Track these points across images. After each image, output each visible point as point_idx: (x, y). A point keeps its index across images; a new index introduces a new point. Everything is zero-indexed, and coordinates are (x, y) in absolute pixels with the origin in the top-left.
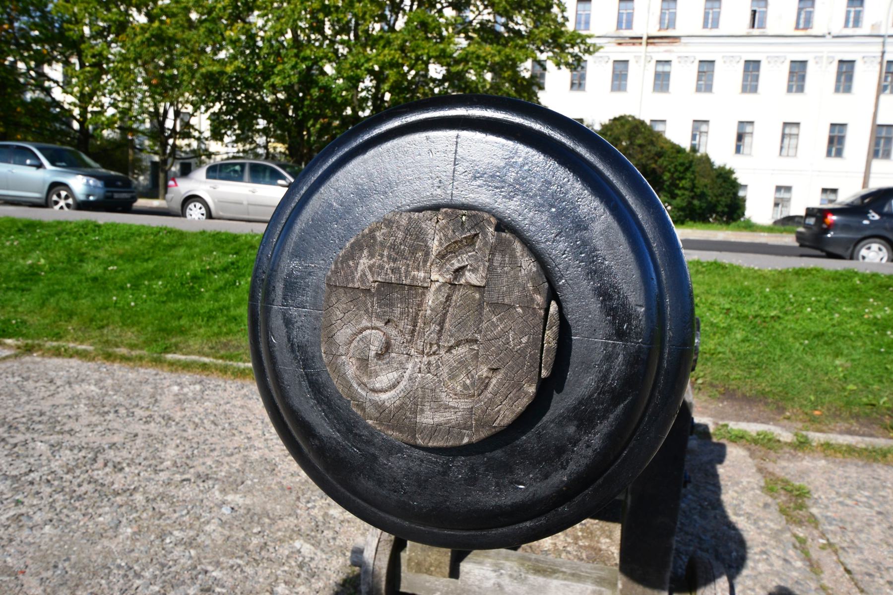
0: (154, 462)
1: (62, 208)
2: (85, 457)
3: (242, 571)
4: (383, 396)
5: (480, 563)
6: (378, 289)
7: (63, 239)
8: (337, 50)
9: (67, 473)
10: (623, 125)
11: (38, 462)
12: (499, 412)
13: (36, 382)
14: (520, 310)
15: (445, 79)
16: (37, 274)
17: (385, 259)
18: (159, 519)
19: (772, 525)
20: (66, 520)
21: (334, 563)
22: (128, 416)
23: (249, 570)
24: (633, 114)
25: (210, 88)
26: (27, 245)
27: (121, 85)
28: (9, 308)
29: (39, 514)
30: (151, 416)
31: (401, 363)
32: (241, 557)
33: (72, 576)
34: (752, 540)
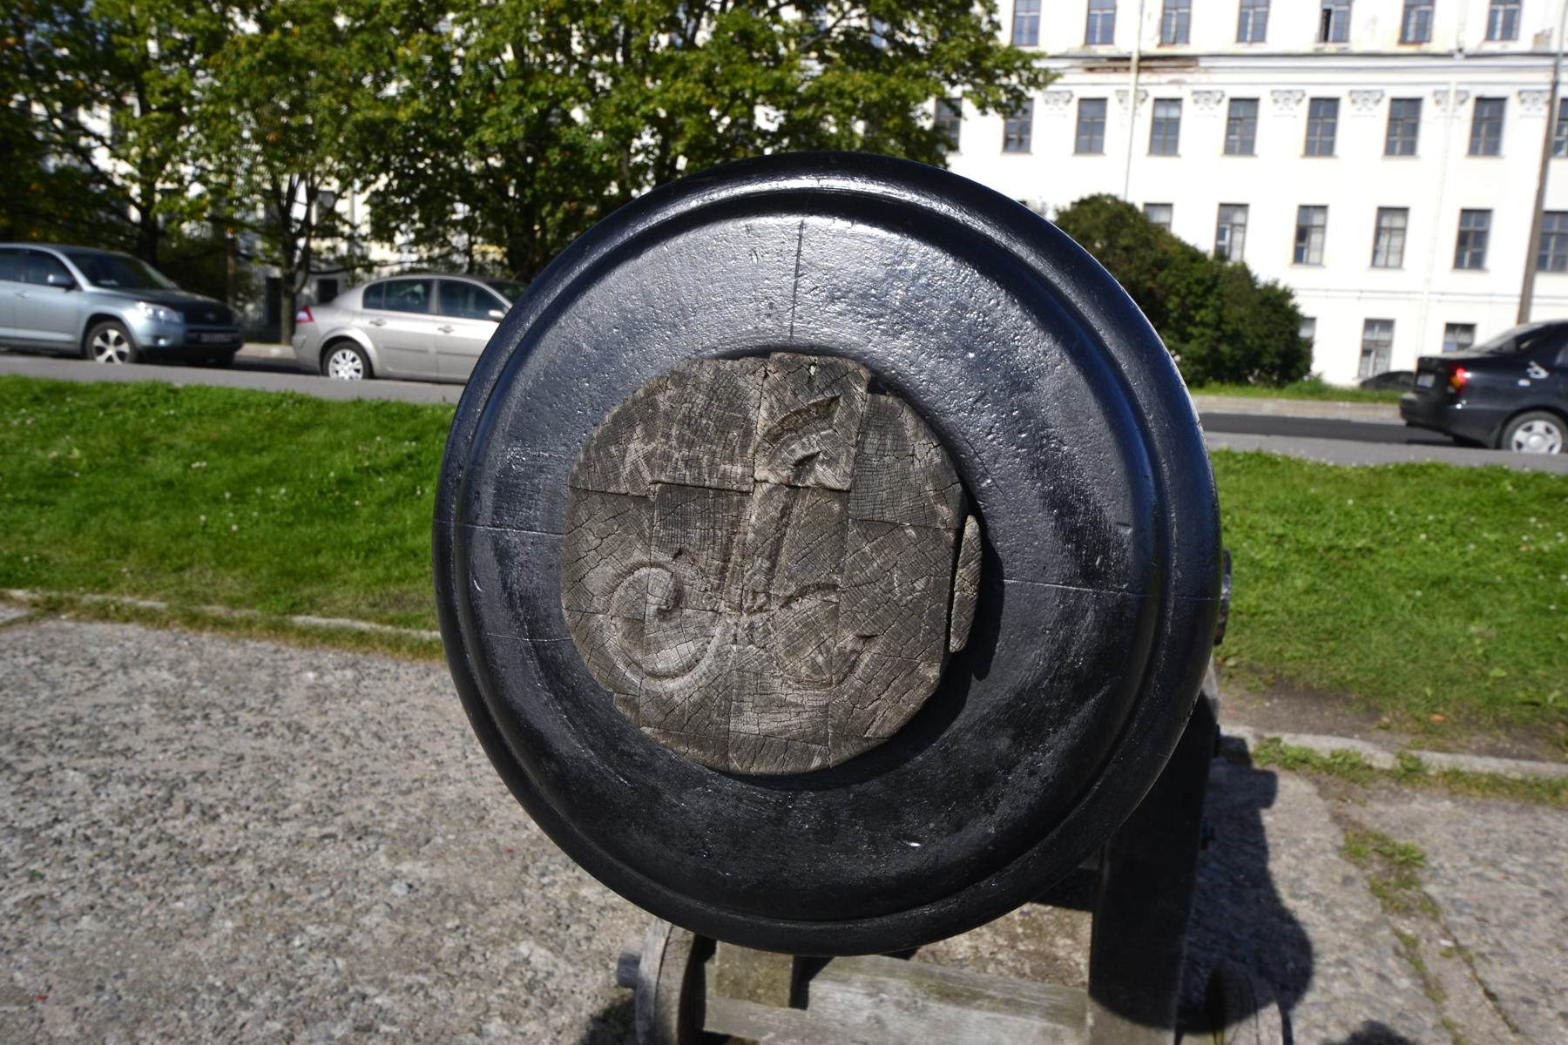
0: (272, 805)
1: (110, 359)
2: (151, 797)
3: (427, 996)
4: (671, 685)
5: (845, 981)
6: (661, 496)
7: (113, 415)
8: (594, 80)
9: (120, 824)
10: (1096, 213)
11: (70, 805)
12: (874, 711)
13: (66, 664)
14: (911, 532)
15: (782, 131)
16: (67, 475)
17: (674, 443)
18: (281, 905)
19: (1357, 915)
20: (118, 906)
21: (589, 981)
22: (226, 724)
23: (440, 994)
24: (1113, 192)
25: (369, 148)
26: (50, 425)
27: (215, 143)
28: (17, 536)
29: (70, 895)
30: (266, 724)
31: (702, 627)
32: (426, 972)
33: (128, 1004)
34: (1323, 941)
